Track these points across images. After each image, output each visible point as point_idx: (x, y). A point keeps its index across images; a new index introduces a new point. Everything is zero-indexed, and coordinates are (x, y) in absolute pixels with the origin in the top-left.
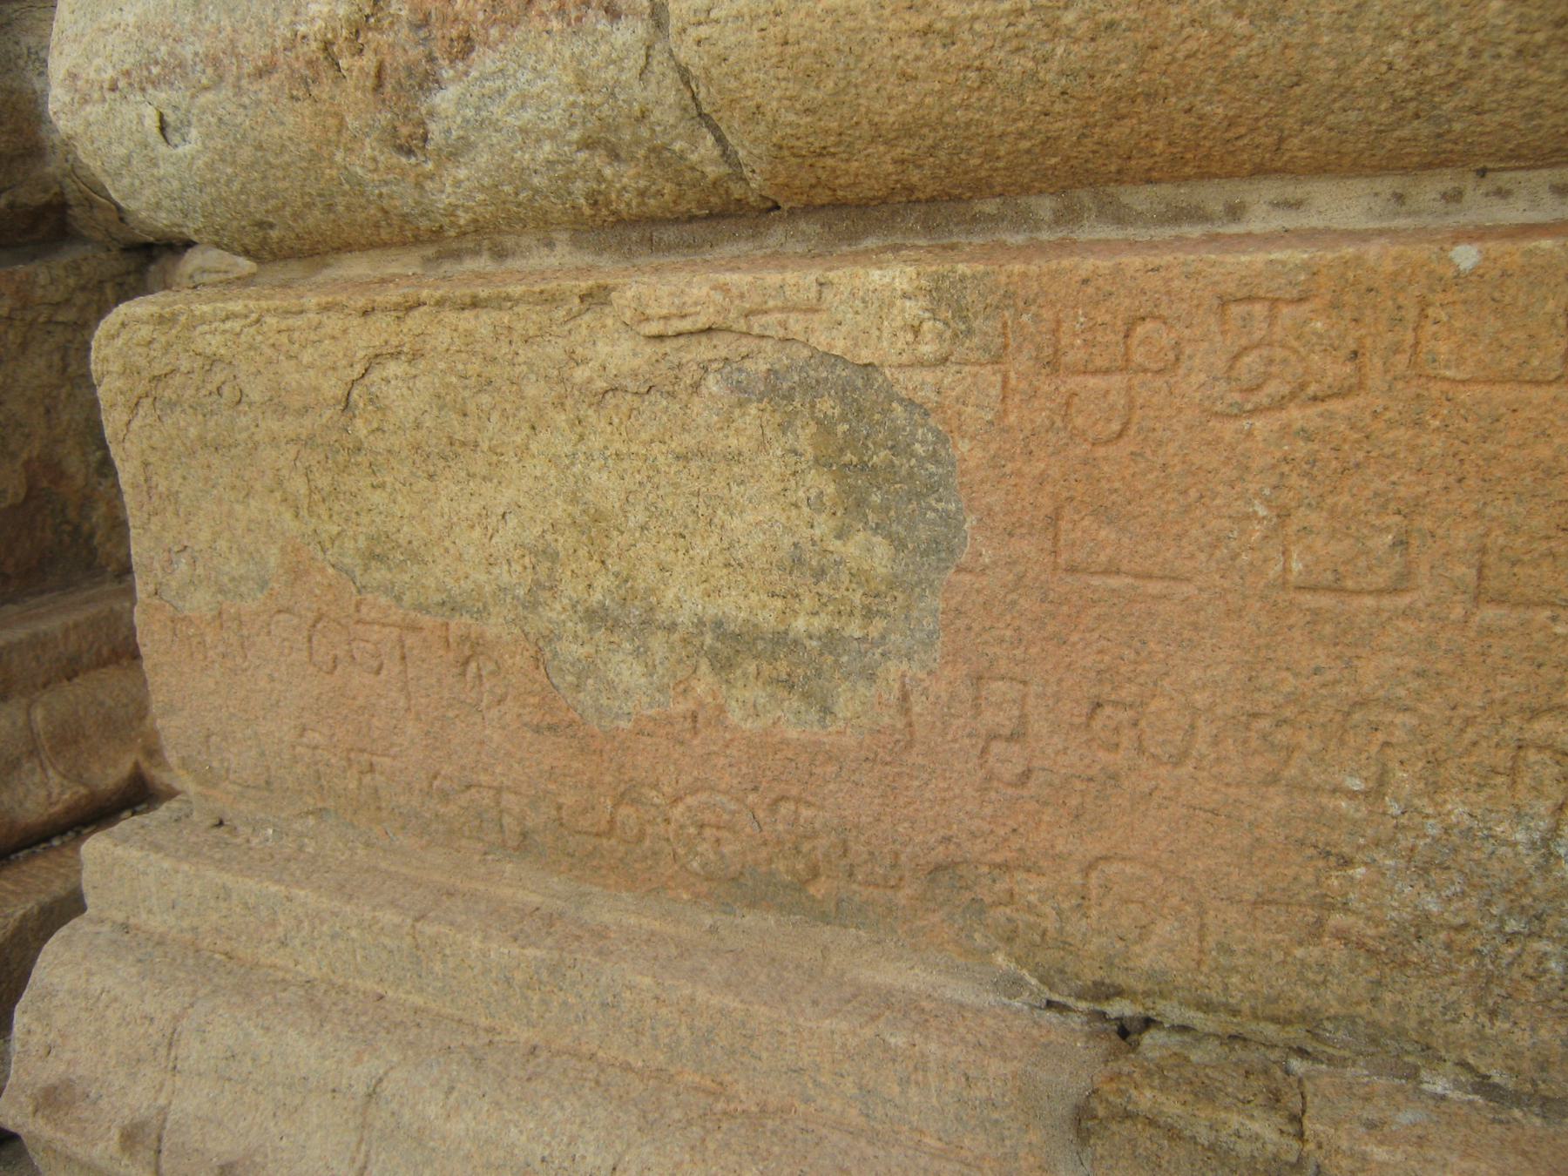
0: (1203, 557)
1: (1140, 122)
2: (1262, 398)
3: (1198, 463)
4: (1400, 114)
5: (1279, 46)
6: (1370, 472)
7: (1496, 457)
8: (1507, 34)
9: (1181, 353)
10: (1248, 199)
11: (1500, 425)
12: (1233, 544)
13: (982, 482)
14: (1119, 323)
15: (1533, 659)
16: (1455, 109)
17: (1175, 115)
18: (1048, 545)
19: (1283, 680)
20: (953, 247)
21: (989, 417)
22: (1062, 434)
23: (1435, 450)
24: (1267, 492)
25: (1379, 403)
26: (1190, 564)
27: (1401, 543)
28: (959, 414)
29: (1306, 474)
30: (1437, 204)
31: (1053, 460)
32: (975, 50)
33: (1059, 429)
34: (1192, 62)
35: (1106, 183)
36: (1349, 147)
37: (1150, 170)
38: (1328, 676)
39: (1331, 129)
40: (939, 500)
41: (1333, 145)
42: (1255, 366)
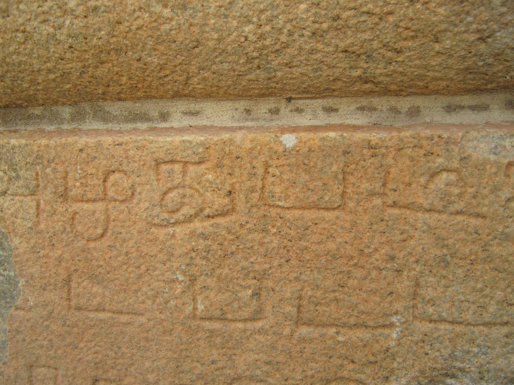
0: (149, 302)
1: (113, 66)
2: (179, 216)
3: (146, 252)
4: (250, 66)
5: (187, 25)
6: (239, 256)
7: (306, 248)
8: (308, 23)
9: (135, 191)
10: (171, 110)
11: (309, 232)
12: (166, 295)
13: (27, 260)
14: (100, 174)
15: (327, 354)
16: (279, 64)
17: (132, 63)
18: (65, 295)
19: (195, 368)
20: (15, 131)
21: (30, 225)
22: (70, 235)
23: (274, 245)
24: (183, 267)
25: (244, 219)
26: (143, 306)
27: (257, 294)
28: (14, 223)
29: (204, 258)
30: (266, 115)
31: (66, 249)
32: (21, 20)
33: (68, 232)
34: (140, 32)
35: (97, 100)
36: (223, 84)
37: (120, 93)
38: (220, 365)
39: (214, 73)
40: (5, 270)
41: (215, 82)
42: (175, 199)
